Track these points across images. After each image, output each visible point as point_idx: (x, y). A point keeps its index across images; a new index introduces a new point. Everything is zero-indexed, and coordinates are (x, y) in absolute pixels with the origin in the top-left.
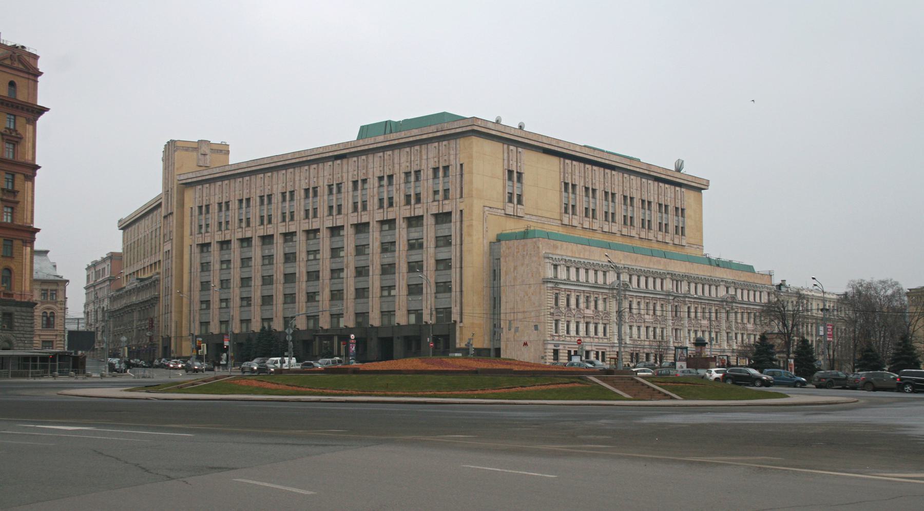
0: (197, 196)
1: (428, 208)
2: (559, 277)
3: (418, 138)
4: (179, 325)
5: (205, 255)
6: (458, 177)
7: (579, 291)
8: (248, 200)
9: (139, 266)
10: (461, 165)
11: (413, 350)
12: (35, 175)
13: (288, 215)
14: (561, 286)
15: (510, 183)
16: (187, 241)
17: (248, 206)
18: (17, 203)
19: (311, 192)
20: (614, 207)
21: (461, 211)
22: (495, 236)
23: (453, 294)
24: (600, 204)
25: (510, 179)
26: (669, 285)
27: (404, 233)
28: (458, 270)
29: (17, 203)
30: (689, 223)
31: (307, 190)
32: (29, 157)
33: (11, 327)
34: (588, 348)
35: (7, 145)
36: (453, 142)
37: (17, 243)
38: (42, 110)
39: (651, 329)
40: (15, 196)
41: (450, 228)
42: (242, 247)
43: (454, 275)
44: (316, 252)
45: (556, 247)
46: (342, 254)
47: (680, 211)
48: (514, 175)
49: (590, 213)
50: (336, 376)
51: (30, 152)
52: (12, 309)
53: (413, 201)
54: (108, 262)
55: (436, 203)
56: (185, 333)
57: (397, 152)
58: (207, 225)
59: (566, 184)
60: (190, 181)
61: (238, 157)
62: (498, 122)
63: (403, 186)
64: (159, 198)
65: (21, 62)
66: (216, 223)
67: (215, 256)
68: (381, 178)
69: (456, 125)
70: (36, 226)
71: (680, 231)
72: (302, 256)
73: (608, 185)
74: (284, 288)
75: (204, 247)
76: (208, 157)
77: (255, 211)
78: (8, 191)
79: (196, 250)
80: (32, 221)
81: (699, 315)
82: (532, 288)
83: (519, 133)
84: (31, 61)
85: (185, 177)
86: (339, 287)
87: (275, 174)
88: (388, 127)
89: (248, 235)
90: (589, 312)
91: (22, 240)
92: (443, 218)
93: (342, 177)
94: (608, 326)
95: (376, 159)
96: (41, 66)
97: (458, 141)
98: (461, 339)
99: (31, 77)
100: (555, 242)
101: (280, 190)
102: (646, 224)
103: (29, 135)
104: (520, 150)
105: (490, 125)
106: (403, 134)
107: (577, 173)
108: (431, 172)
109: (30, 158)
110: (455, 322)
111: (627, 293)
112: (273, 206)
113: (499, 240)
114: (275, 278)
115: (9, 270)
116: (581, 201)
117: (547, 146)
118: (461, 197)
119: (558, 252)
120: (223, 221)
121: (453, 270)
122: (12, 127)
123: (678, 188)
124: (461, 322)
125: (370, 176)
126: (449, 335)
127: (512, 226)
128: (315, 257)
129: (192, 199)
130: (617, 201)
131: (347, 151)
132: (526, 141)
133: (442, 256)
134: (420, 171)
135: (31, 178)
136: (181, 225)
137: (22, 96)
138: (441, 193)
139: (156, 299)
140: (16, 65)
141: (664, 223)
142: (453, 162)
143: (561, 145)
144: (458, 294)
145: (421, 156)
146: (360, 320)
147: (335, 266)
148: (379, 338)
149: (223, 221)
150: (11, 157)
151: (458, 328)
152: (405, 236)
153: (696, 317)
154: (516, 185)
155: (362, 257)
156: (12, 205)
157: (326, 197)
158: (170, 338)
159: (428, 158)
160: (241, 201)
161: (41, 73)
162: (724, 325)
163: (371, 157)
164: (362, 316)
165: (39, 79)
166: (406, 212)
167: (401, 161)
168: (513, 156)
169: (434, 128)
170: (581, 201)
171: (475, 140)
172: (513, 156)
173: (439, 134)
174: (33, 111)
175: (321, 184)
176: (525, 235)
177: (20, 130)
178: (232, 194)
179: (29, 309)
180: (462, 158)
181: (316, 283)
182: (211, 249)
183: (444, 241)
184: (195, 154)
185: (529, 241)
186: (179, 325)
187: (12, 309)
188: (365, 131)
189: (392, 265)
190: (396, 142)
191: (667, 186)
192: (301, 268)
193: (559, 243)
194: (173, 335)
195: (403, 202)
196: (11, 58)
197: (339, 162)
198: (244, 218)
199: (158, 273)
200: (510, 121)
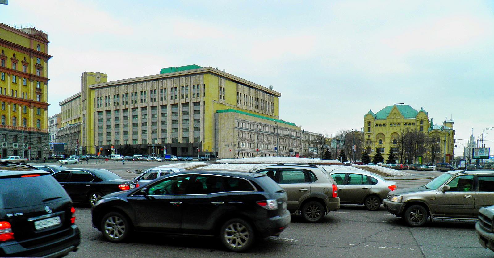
0: (97, 93)
1: (191, 100)
2: (240, 126)
3: (187, 74)
4: (90, 142)
5: (100, 115)
6: (203, 89)
7: (246, 132)
8: (118, 95)
9: (69, 119)
10: (204, 84)
11: (185, 152)
12: (48, 82)
13: (134, 101)
14: (240, 130)
15: (221, 92)
16: (93, 110)
17: (118, 97)
18: (42, 94)
19: (125, 95)
20: (253, 102)
21: (204, 101)
22: (216, 111)
23: (201, 132)
24: (248, 100)
25: (221, 90)
26: (272, 130)
27: (181, 109)
28: (203, 123)
29: (42, 94)
30: (275, 108)
31: (142, 92)
32: (45, 76)
33: (41, 143)
34: (282, 154)
35: (37, 70)
36: (201, 76)
37: (42, 109)
38: (50, 57)
39: (267, 145)
40: (41, 91)
41: (200, 107)
42: (115, 113)
43: (201, 125)
44: (145, 115)
45: (238, 115)
46: (156, 116)
47: (272, 104)
48: (222, 89)
49: (245, 103)
50: (225, 169)
51: (46, 74)
52: (41, 136)
53: (185, 97)
54: (56, 118)
55: (194, 98)
56: (92, 144)
57: (178, 78)
58: (101, 105)
59: (238, 93)
60: (94, 87)
61: (111, 79)
62: (217, 69)
63: (181, 91)
64: (80, 93)
65: (41, 37)
66: (105, 104)
67: (104, 116)
68: (172, 88)
69: (198, 69)
70: (48, 103)
71: (272, 111)
72: (140, 117)
73: (251, 93)
74: (133, 129)
75: (100, 113)
76: (100, 78)
77: (120, 100)
78: (38, 89)
79: (97, 114)
80: (47, 101)
81: (281, 140)
82: (231, 130)
83: (223, 73)
84: (45, 36)
85: (92, 86)
86: (155, 128)
87: (129, 85)
88: (176, 69)
89: (118, 108)
90: (249, 139)
91: (44, 108)
92: (197, 103)
93: (156, 87)
94: (254, 144)
95: (170, 81)
96: (49, 39)
97: (203, 75)
98: (204, 148)
99: (45, 43)
100: (239, 114)
101: (131, 91)
102: (262, 108)
103: (45, 67)
104: (224, 79)
105: (215, 70)
106: (181, 72)
107: (242, 89)
108: (192, 87)
109: (46, 76)
110: (202, 142)
111: (260, 132)
112: (128, 98)
113: (217, 112)
114: (129, 124)
115: (39, 120)
116: (243, 99)
117: (232, 79)
118: (204, 96)
119: (239, 117)
120: (107, 103)
121: (201, 123)
122: (39, 63)
123: (272, 96)
124: (204, 142)
125: (168, 87)
126: (188, 147)
127: (221, 108)
128: (145, 117)
129: (94, 94)
130: (253, 99)
131: (159, 78)
132: (226, 76)
133: (196, 118)
134: (177, 87)
135: (46, 84)
136: (90, 104)
137: (42, 51)
138: (196, 94)
139: (79, 132)
140: (40, 38)
141: (262, 106)
142: (201, 83)
143: (237, 78)
144: (203, 132)
145: (188, 80)
146: (163, 141)
147: (153, 121)
148: (171, 148)
149: (107, 103)
150: (39, 75)
151: (203, 144)
152: (182, 110)
153: (280, 141)
154: (223, 92)
155: (164, 118)
156: (40, 95)
157: (150, 95)
158: (86, 147)
159: (191, 81)
160: (115, 95)
161: (49, 42)
162: (288, 144)
163: (168, 80)
164: (175, 140)
165: (49, 44)
166: (182, 101)
167: (180, 82)
168: (222, 81)
169: (194, 70)
170: (243, 99)
171: (209, 75)
172: (222, 81)
173: (195, 72)
174: (47, 57)
175: (148, 90)
176: (228, 111)
177: (42, 65)
178: (111, 93)
179: (47, 136)
180: (205, 82)
181: (146, 127)
182: (103, 113)
183: (197, 112)
184: (95, 77)
185: (230, 113)
186: (90, 142)
187: (41, 136)
188: (163, 71)
189: (176, 121)
190: (179, 75)
191: (268, 95)
192: (139, 121)
193: (240, 114)
194: (87, 146)
195: (181, 97)
196: (38, 35)
197: (155, 81)
198: (116, 102)
199: (80, 122)
200: (221, 69)
